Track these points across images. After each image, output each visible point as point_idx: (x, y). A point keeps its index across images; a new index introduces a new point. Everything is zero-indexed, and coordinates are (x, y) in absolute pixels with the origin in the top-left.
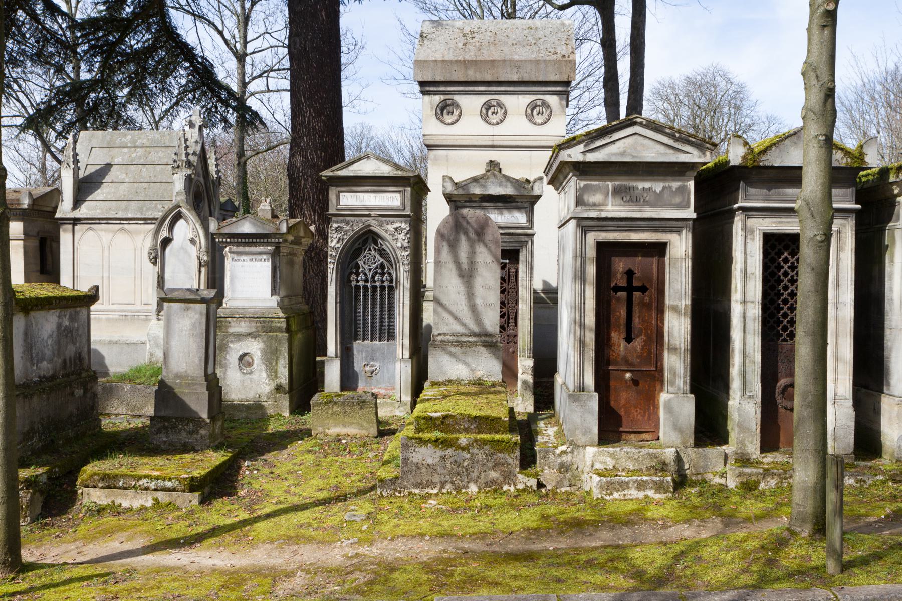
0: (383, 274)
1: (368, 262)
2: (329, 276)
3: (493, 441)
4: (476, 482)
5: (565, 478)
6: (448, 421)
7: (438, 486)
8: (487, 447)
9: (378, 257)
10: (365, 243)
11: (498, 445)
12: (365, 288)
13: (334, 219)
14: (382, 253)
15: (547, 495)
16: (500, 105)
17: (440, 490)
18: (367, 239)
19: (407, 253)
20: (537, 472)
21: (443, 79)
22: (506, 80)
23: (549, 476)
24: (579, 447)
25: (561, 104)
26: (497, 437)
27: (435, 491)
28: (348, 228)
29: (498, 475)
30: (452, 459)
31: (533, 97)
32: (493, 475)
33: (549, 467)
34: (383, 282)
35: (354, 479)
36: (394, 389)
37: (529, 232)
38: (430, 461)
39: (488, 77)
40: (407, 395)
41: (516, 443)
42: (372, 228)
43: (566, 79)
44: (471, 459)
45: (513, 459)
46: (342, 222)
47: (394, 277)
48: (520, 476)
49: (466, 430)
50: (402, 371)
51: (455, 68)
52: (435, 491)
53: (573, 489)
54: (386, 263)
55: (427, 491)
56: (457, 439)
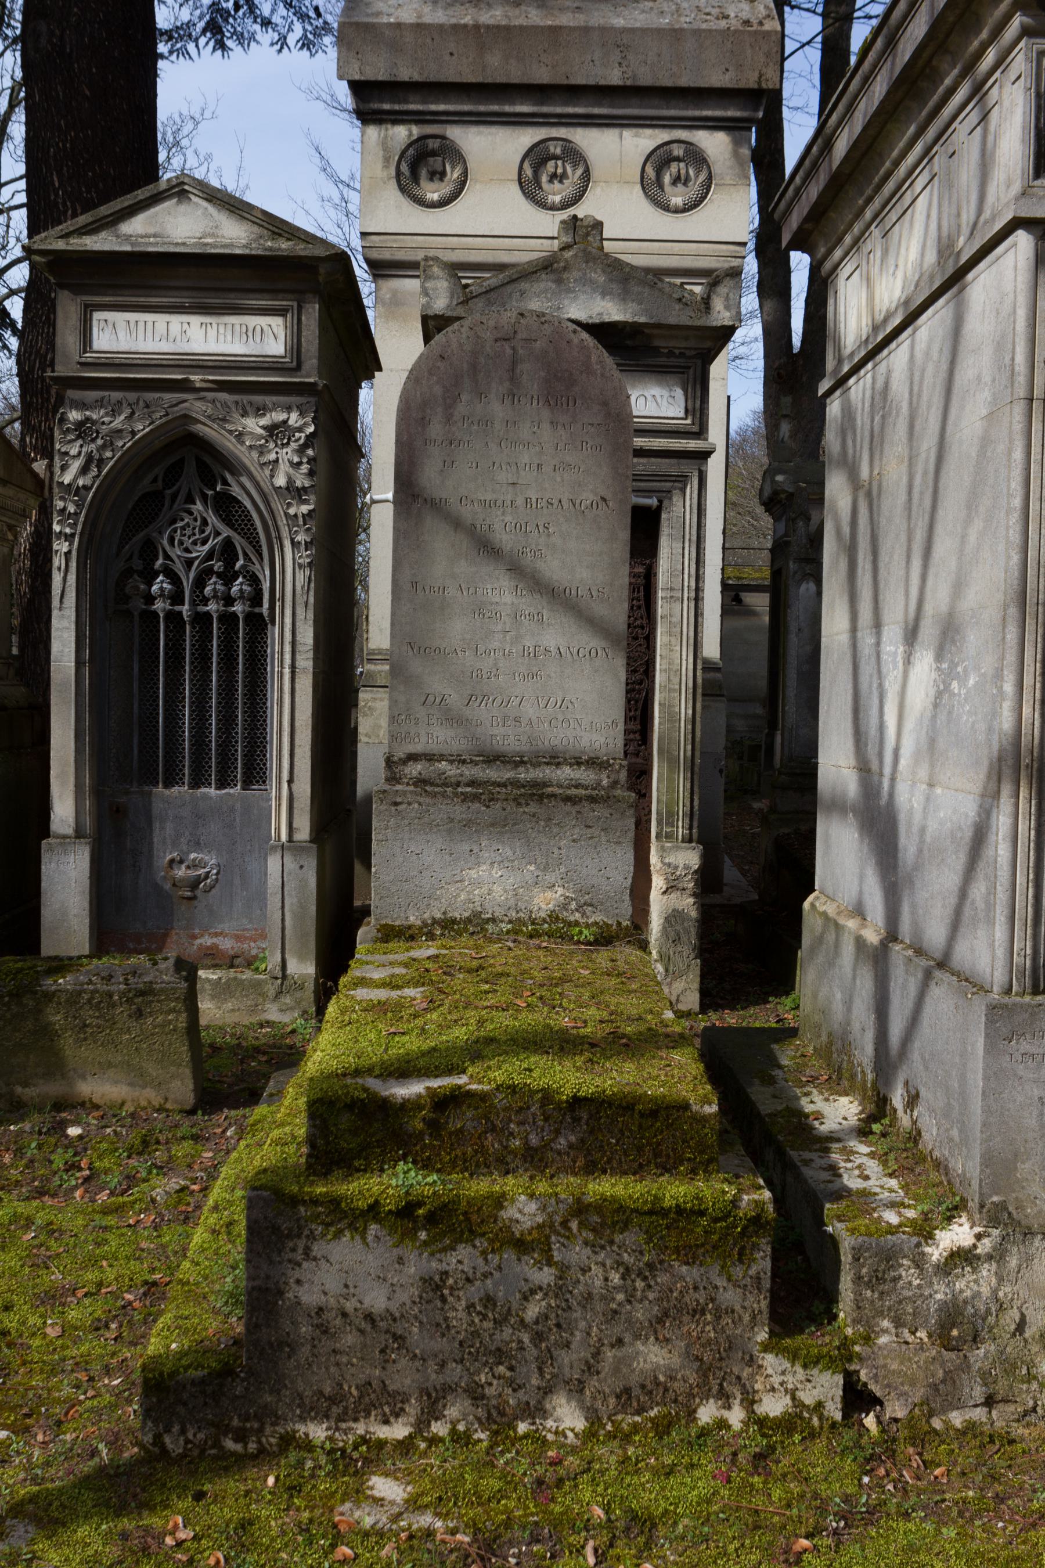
0: (228, 577)
1: (192, 538)
2: (57, 578)
3: (656, 1211)
4: (577, 1390)
5: (965, 1365)
6: (458, 1121)
7: (413, 1408)
8: (632, 1238)
9: (212, 519)
10: (174, 473)
11: (675, 1230)
12: (174, 617)
13: (71, 394)
14: (227, 507)
15: (888, 1443)
16: (574, 155)
17: (421, 1425)
18: (180, 464)
19: (305, 509)
20: (846, 1344)
21: (417, 78)
22: (591, 82)
23: (896, 1355)
24: (1028, 1233)
25: (736, 154)
26: (675, 1191)
27: (399, 1431)
28: (118, 422)
29: (676, 1361)
30: (474, 1292)
31: (663, 136)
32: (653, 1357)
33: (898, 1323)
34: (229, 601)
35: (73, 1315)
36: (263, 936)
37: (692, 445)
38: (377, 1300)
39: (542, 75)
40: (302, 958)
41: (756, 1222)
42: (199, 428)
43: (753, 85)
44: (559, 1290)
45: (742, 1292)
46: (100, 403)
47: (266, 586)
48: (769, 1360)
49: (536, 1160)
50: (286, 882)
51: (452, 46)
52: (399, 1431)
53: (1000, 1418)
54: (238, 541)
55: (360, 1428)
56: (499, 1201)
